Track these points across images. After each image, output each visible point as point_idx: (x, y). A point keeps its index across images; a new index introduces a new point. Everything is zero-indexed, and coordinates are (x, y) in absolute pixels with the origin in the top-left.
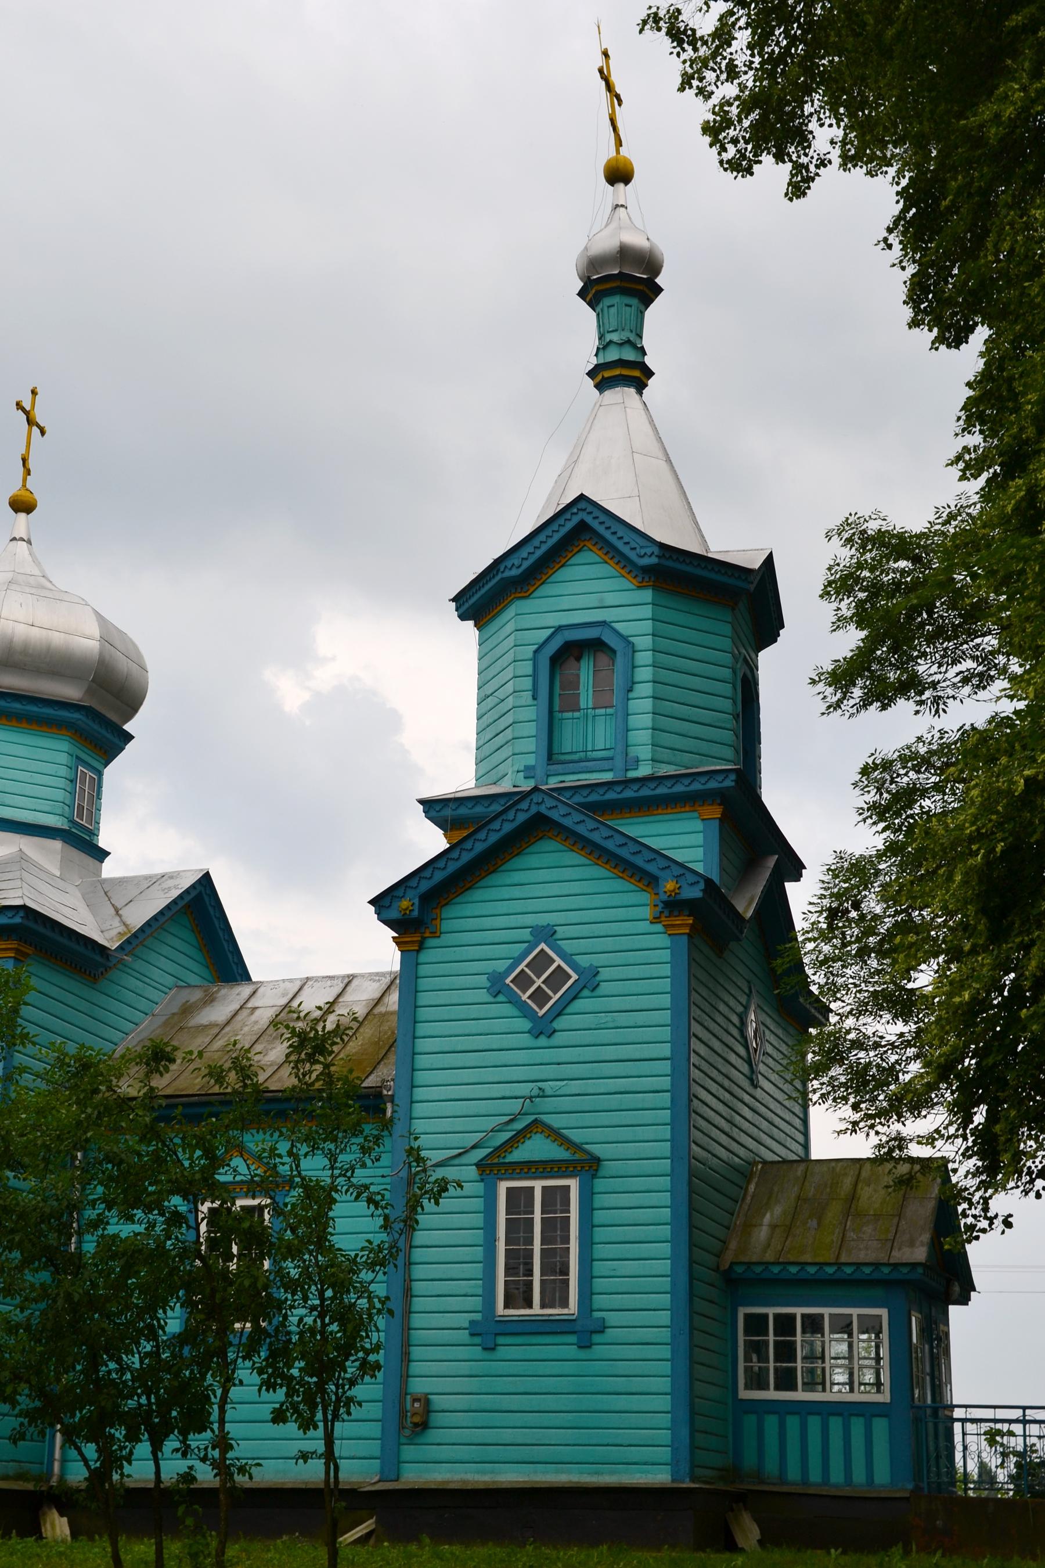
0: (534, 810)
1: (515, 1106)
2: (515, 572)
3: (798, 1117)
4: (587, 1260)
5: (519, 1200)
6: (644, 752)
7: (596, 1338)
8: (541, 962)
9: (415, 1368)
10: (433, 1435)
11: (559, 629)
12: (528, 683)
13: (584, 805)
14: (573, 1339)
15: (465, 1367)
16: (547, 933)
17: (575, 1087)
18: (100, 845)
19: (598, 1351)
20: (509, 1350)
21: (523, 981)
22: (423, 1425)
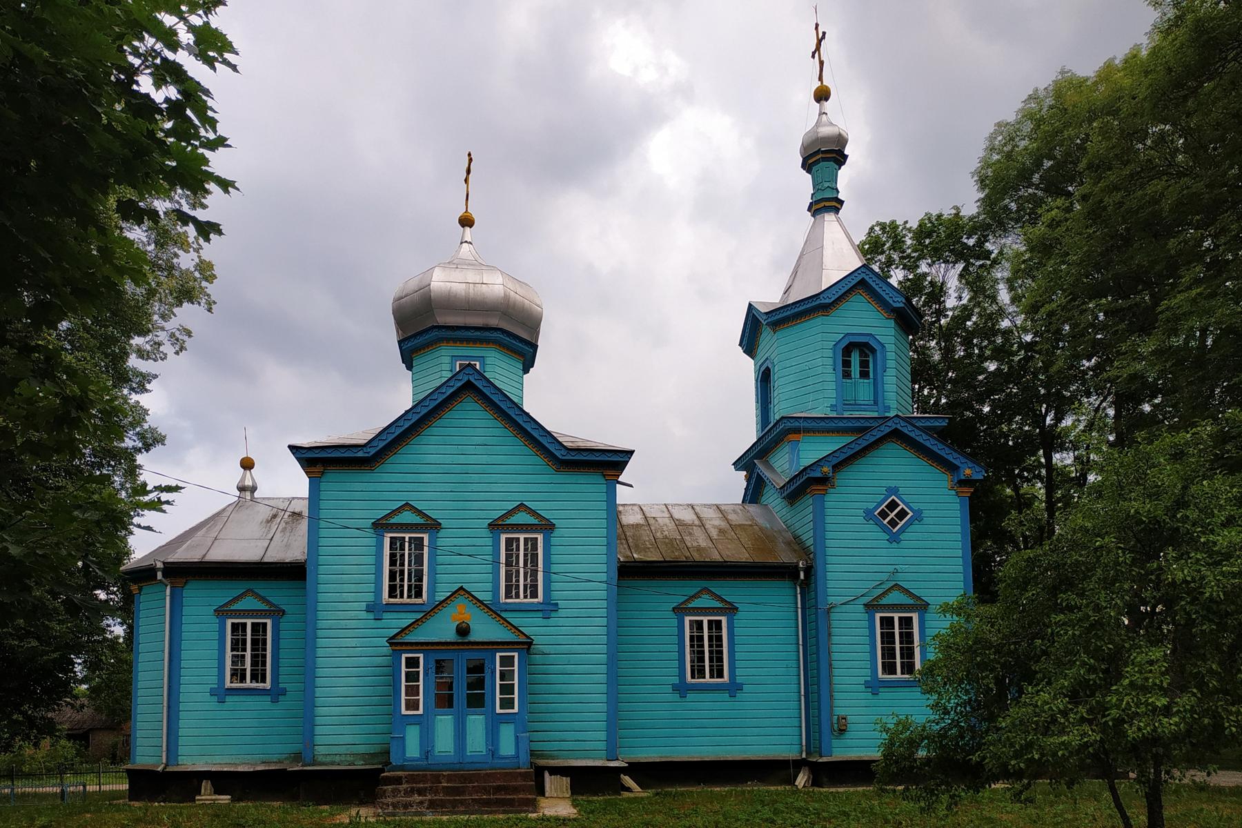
0: (894, 427)
1: (884, 577)
2: (828, 301)
3: (229, 603)
4: (496, 573)
5: (886, 622)
6: (893, 404)
7: (553, 614)
8: (892, 505)
9: (837, 703)
10: (847, 735)
11: (848, 334)
12: (830, 361)
13: (926, 428)
14: (540, 614)
15: (863, 703)
16: (893, 491)
17: (913, 569)
18: (530, 406)
19: (552, 621)
20: (885, 694)
21: (883, 515)
22: (842, 731)
